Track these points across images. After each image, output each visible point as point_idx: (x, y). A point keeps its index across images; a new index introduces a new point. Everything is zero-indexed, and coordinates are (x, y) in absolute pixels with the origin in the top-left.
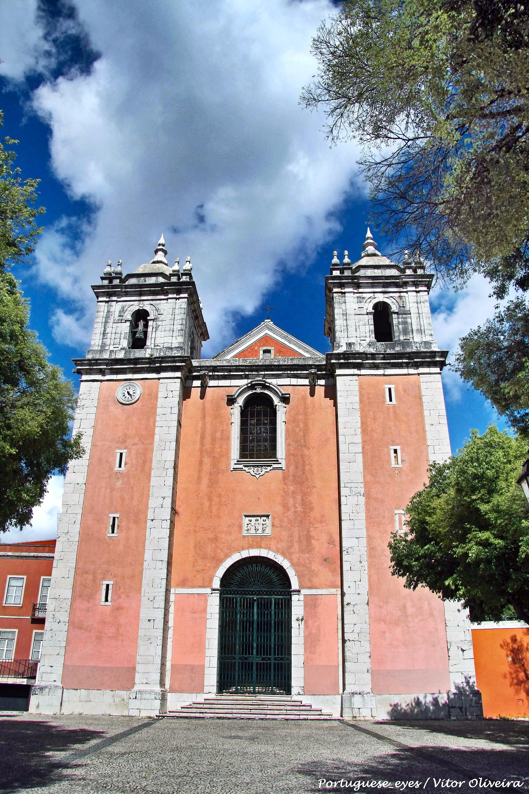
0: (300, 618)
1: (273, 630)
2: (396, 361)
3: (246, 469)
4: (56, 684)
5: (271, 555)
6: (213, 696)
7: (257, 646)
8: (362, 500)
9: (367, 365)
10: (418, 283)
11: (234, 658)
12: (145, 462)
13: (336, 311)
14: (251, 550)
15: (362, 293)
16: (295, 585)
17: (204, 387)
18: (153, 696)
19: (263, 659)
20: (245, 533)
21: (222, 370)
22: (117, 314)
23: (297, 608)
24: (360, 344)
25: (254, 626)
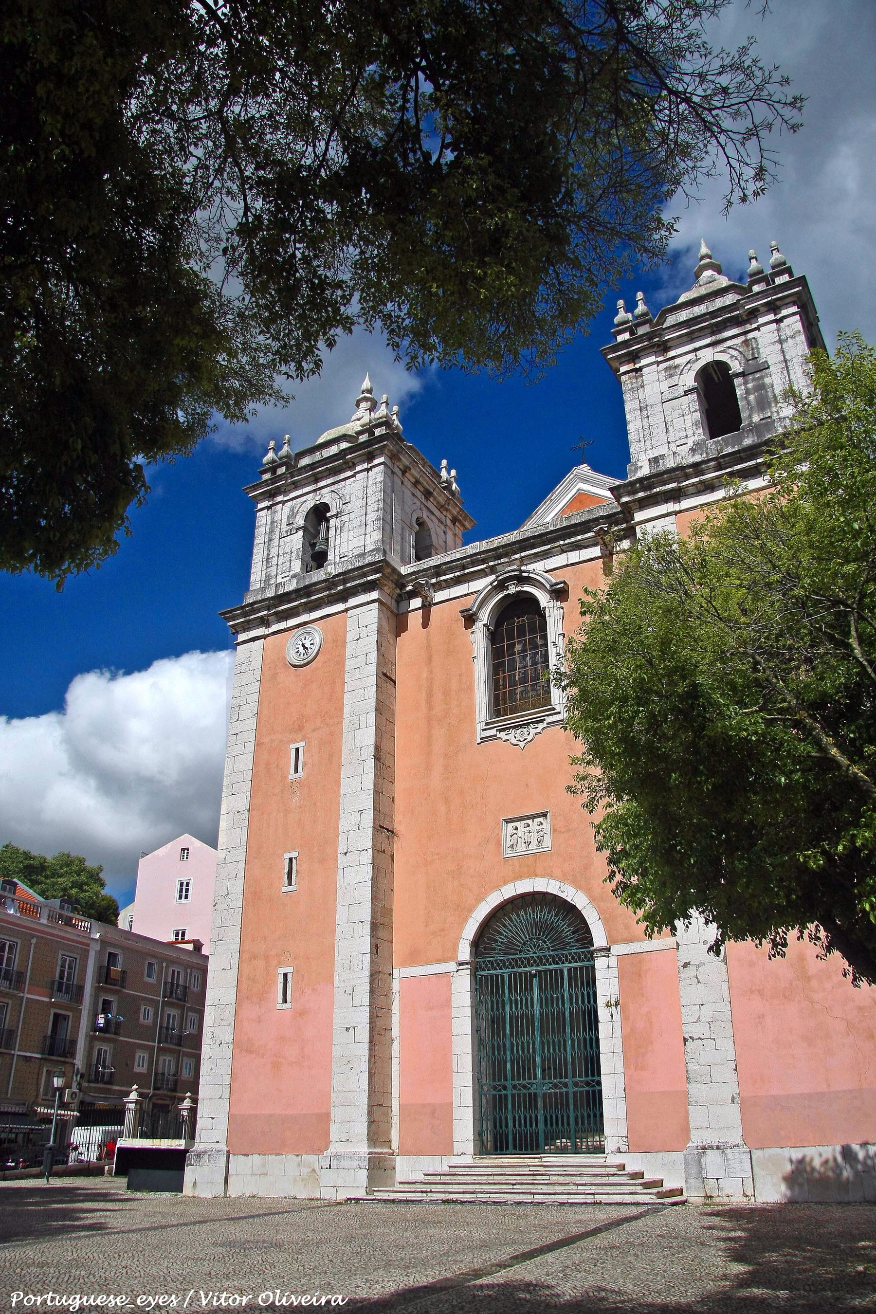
0: (613, 1002)
1: (568, 1030)
2: (745, 465)
3: (503, 735)
4: (217, 1146)
5: (552, 887)
6: (468, 1160)
7: (543, 1060)
9: (692, 490)
10: (778, 303)
11: (505, 1088)
12: (331, 755)
13: (627, 407)
14: (518, 883)
15: (673, 358)
16: (599, 939)
17: (426, 607)
18: (355, 1164)
19: (555, 1086)
20: (509, 853)
21: (452, 570)
22: (285, 522)
24: (674, 453)
25: (536, 1024)
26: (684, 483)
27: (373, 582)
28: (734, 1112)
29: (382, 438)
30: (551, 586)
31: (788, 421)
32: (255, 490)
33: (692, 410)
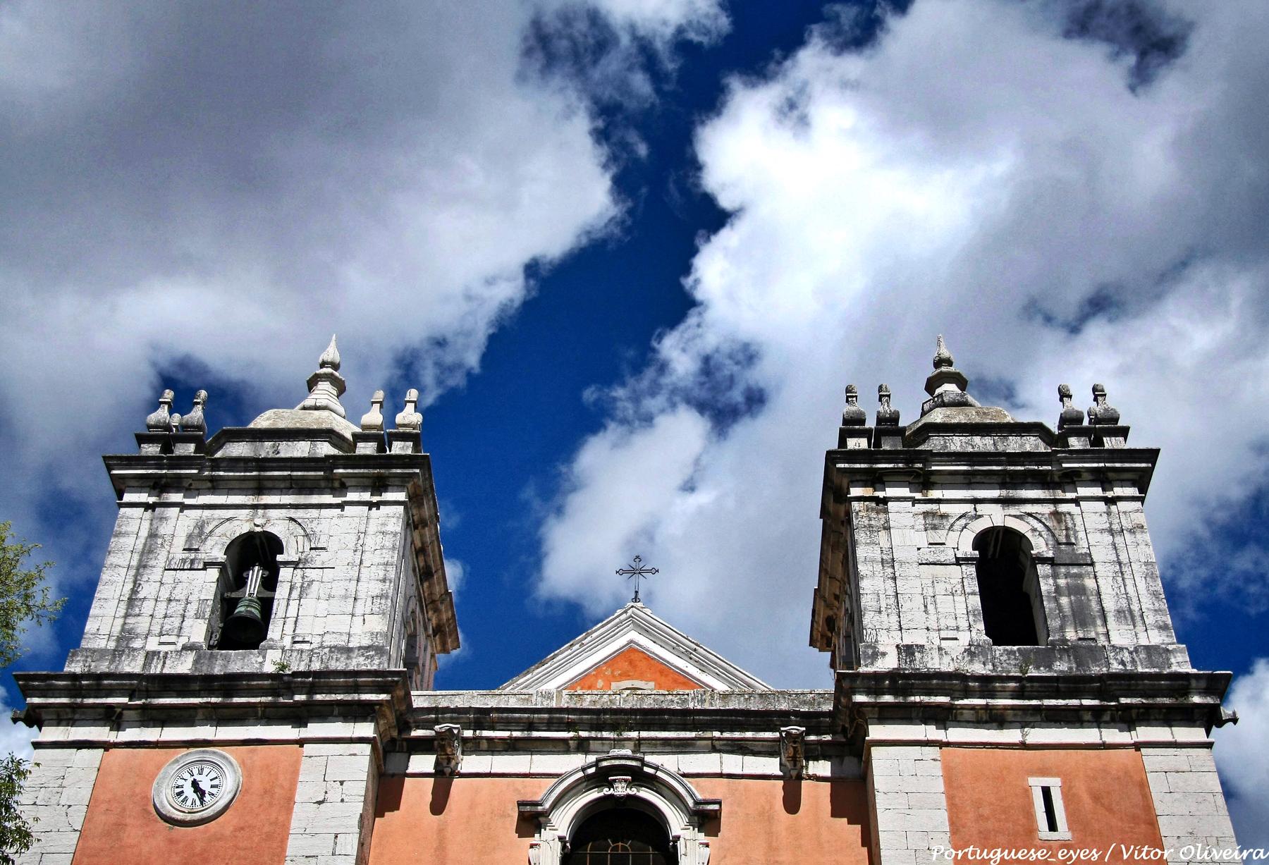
2: (1061, 702)
9: (968, 715)
10: (1111, 475)
13: (861, 552)
15: (938, 501)
17: (444, 776)
21: (507, 725)
22: (180, 542)
26: (961, 702)
27: (371, 704)
29: (401, 461)
30: (697, 803)
31: (1127, 654)
32: (129, 467)
33: (968, 590)
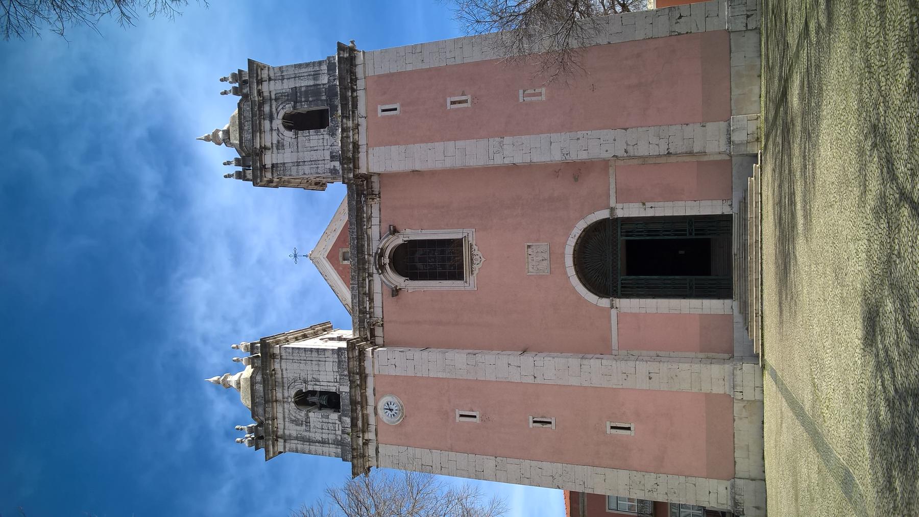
8: (508, 140)
16: (604, 214)
22: (299, 428)
23: (632, 210)
28: (710, 126)
